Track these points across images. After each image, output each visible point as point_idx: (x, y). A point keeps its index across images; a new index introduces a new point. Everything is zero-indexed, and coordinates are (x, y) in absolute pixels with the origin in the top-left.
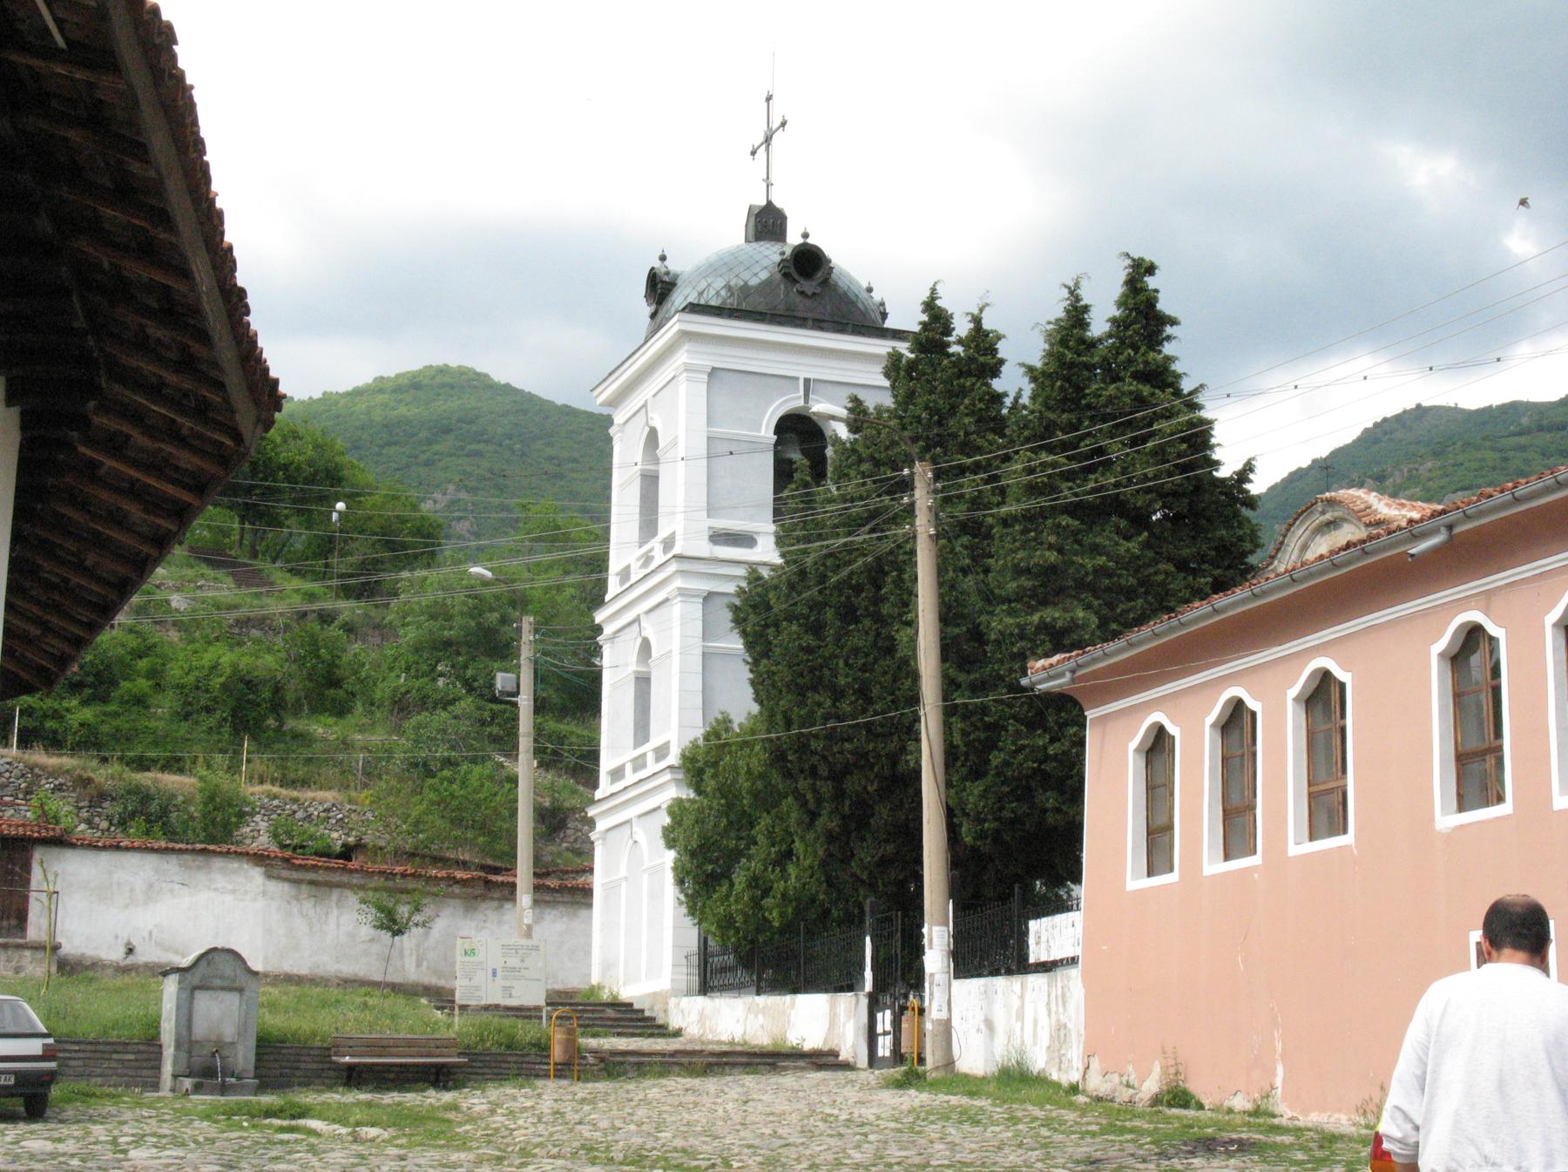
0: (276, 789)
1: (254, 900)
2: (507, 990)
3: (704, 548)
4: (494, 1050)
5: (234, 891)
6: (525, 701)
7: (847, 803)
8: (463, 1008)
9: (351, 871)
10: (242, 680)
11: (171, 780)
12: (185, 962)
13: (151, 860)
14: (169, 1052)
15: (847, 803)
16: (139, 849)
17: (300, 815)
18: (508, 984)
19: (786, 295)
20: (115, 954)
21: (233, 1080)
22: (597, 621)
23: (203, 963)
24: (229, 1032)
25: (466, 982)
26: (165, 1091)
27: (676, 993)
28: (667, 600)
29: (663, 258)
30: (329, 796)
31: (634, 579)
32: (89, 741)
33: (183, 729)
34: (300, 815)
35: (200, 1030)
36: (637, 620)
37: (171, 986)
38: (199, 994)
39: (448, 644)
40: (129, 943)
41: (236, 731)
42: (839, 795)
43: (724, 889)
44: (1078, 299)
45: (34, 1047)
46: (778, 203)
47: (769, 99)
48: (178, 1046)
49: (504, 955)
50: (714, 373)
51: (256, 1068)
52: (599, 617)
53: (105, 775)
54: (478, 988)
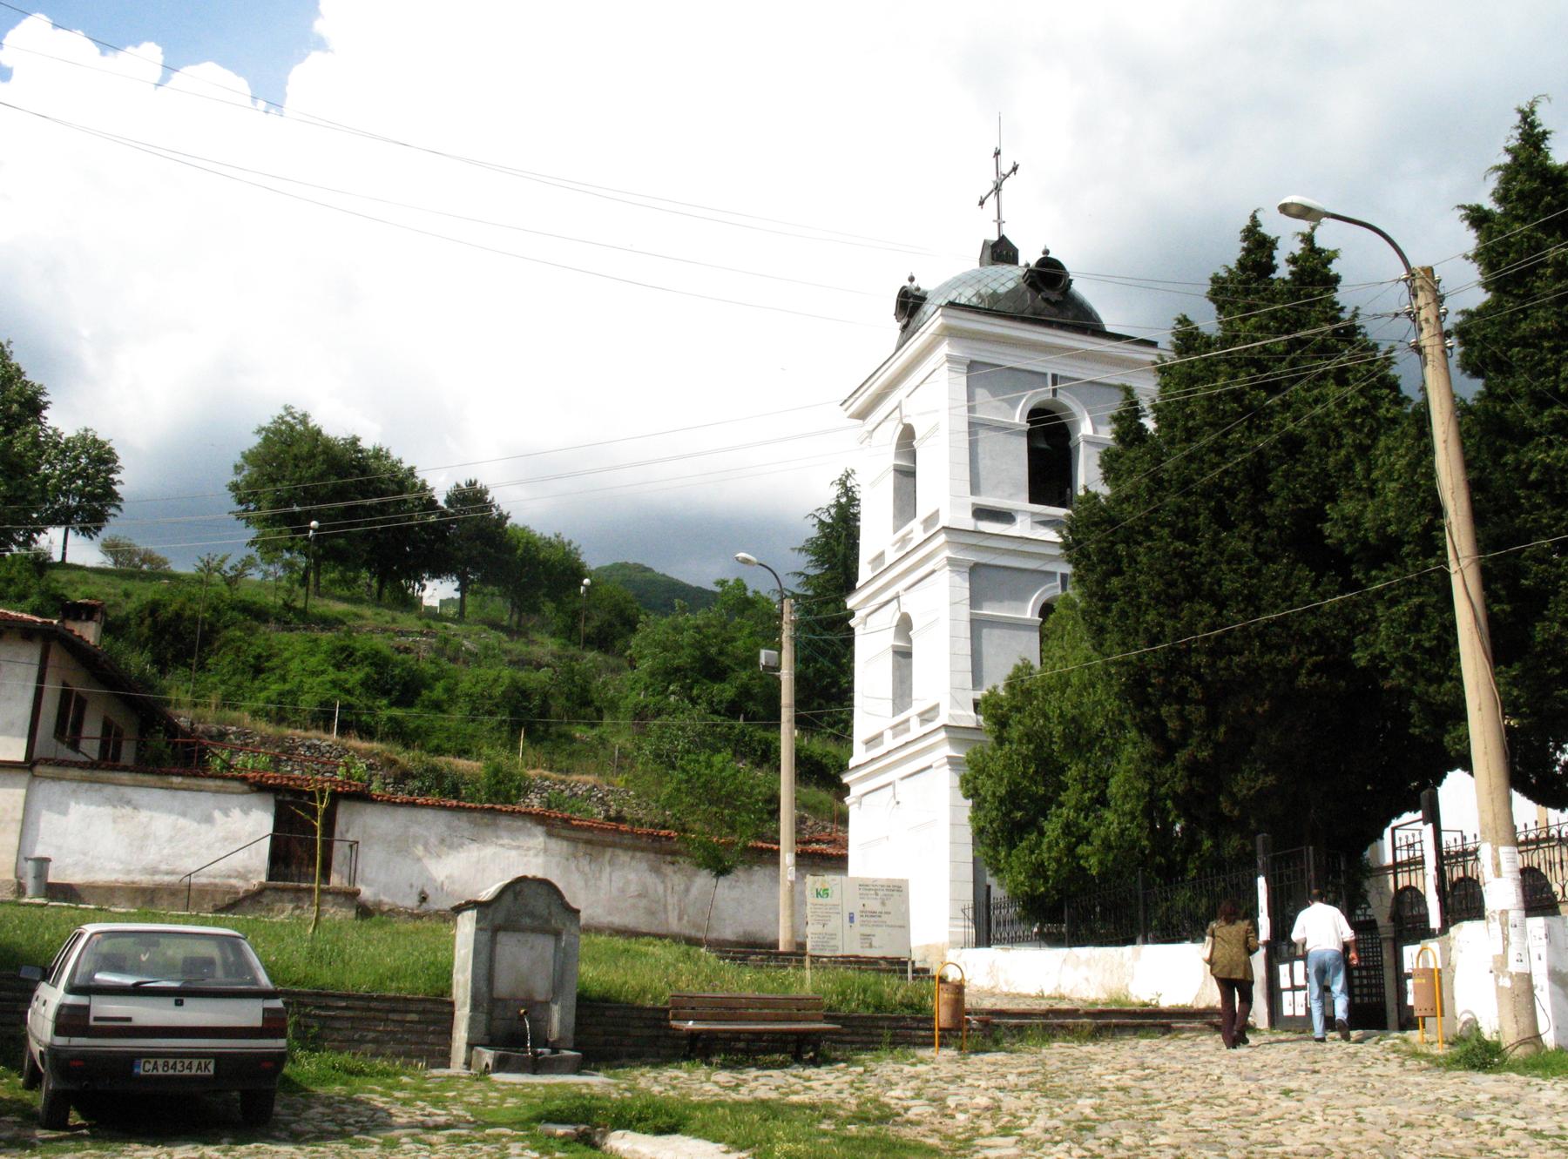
0: (546, 773)
1: (536, 855)
2: (866, 938)
3: (968, 522)
4: (865, 1013)
5: (518, 847)
6: (786, 676)
7: (1222, 729)
8: (816, 959)
9: (623, 833)
10: (518, 689)
11: (462, 764)
12: (487, 894)
13: (443, 816)
14: (462, 1015)
15: (1222, 729)
16: (432, 806)
17: (567, 793)
18: (867, 930)
19: (1033, 300)
20: (411, 902)
21: (546, 1051)
22: (849, 605)
23: (509, 897)
24: (541, 987)
25: (819, 928)
26: (457, 1066)
27: (954, 944)
28: (933, 572)
29: (912, 279)
30: (591, 779)
31: (888, 561)
32: (401, 734)
33: (471, 728)
34: (567, 793)
35: (503, 986)
36: (897, 597)
37: (467, 925)
38: (502, 937)
39: (678, 669)
40: (422, 892)
41: (514, 733)
42: (1212, 721)
43: (1034, 836)
44: (1532, 126)
45: (249, 1013)
46: (1013, 239)
47: (997, 154)
48: (475, 1007)
49: (862, 896)
50: (972, 366)
51: (576, 1034)
52: (851, 603)
53: (408, 758)
54: (833, 936)
